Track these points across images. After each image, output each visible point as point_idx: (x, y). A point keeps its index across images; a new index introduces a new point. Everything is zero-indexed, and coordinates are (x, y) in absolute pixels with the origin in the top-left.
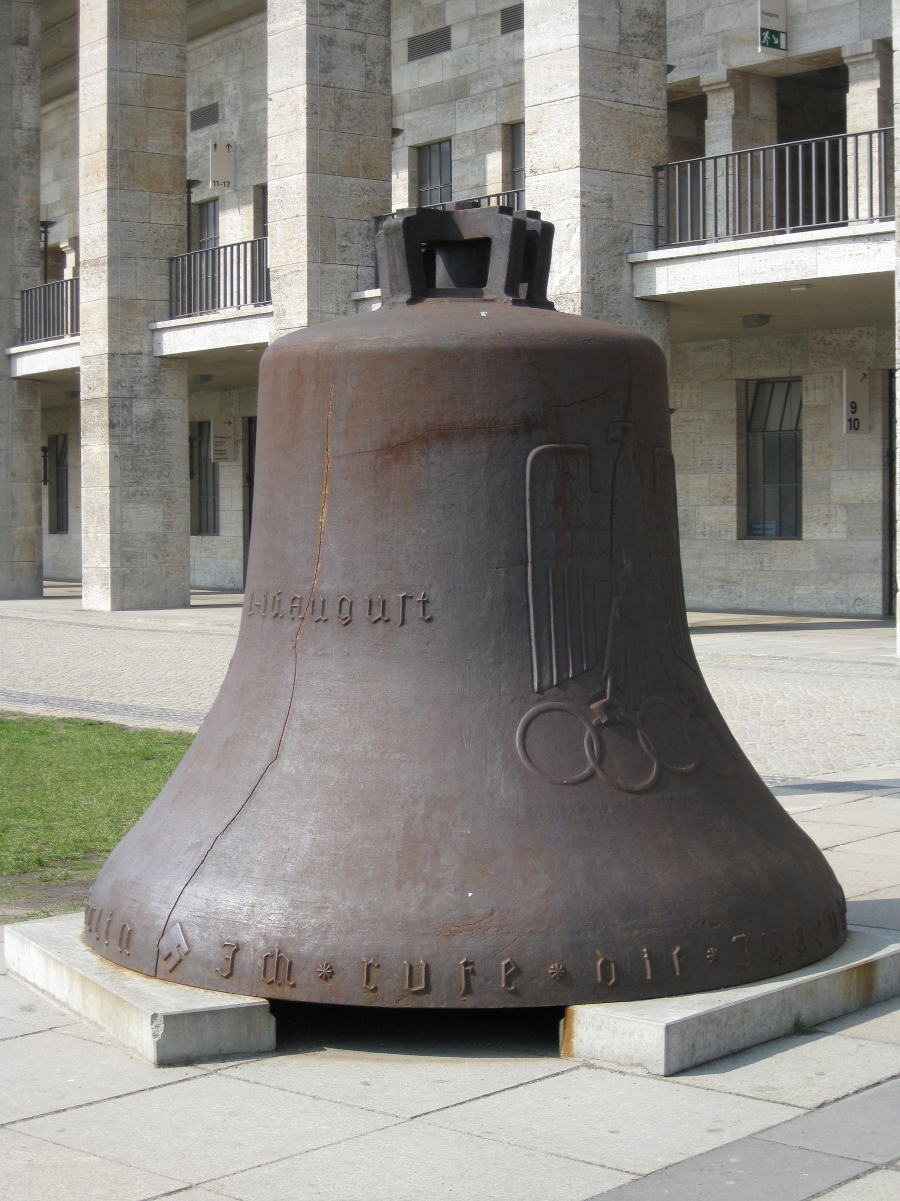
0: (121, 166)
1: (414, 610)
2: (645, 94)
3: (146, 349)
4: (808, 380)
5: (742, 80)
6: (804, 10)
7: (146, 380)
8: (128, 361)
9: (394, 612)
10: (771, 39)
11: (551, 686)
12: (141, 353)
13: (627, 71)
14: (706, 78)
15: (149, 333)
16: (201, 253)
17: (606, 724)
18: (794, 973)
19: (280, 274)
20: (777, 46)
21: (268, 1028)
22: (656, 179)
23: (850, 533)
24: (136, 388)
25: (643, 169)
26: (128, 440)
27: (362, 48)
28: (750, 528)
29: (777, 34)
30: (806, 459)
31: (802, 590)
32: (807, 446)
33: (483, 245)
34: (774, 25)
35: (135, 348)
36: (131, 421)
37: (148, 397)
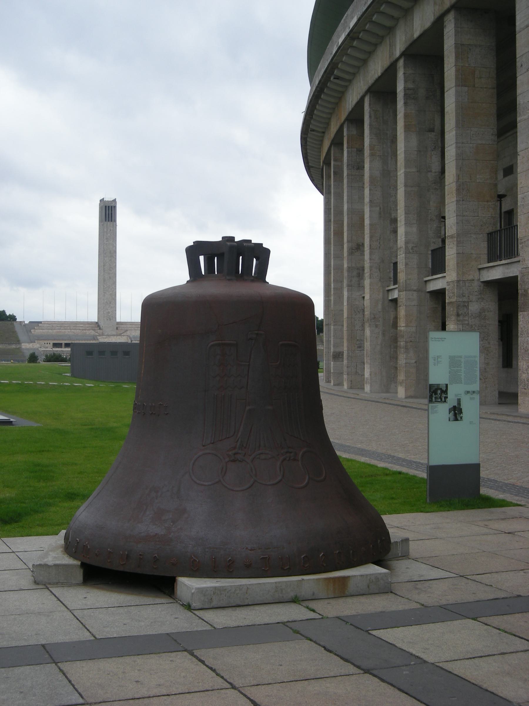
0: (463, 189)
3: (476, 278)
7: (476, 293)
8: (467, 284)
12: (473, 280)
15: (477, 271)
16: (509, 228)
19: (523, 241)
21: (79, 575)
24: (471, 297)
26: (466, 322)
35: (471, 277)
36: (468, 313)
37: (477, 301)
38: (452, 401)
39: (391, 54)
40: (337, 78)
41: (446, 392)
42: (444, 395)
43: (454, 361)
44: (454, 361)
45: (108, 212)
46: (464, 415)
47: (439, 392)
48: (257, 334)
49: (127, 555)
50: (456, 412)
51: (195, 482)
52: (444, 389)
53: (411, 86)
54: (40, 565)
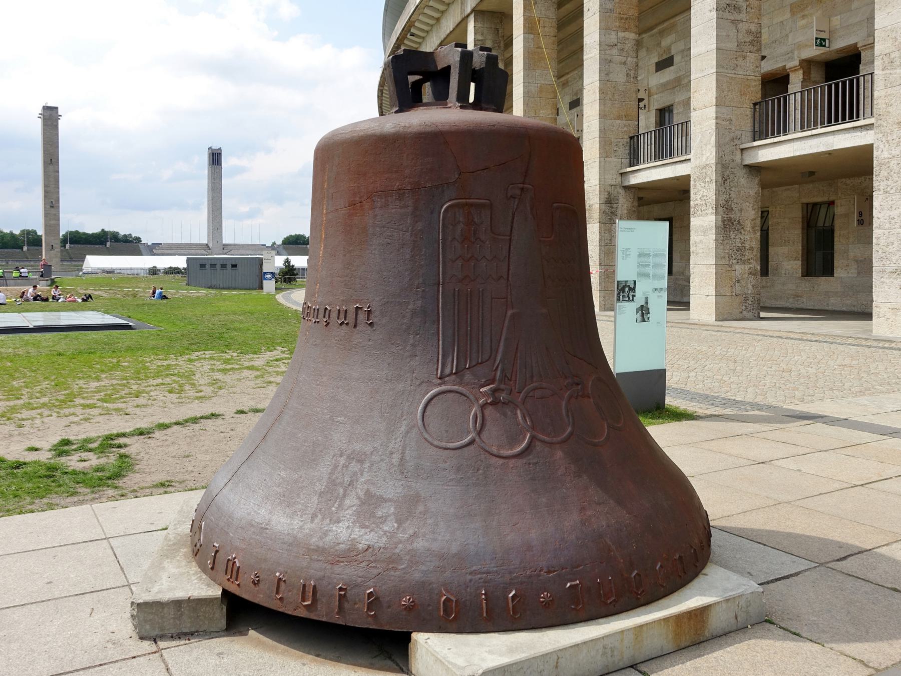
1: (362, 317)
2: (752, 70)
4: (838, 202)
5: (807, 65)
6: (838, 27)
9: (351, 318)
10: (821, 42)
11: (451, 374)
13: (740, 59)
14: (789, 65)
17: (491, 404)
18: (630, 612)
20: (825, 46)
21: (220, 616)
22: (755, 109)
23: (859, 273)
25: (748, 105)
27: (625, 63)
28: (808, 272)
29: (824, 40)
30: (836, 239)
31: (833, 301)
32: (836, 234)
33: (447, 69)
34: (822, 36)
38: (639, 300)
39: (463, 10)
40: (413, 35)
41: (633, 289)
42: (631, 294)
43: (643, 255)
44: (643, 255)
45: (215, 158)
46: (651, 315)
47: (627, 289)
48: (522, 189)
49: (314, 587)
50: (644, 312)
51: (432, 444)
52: (632, 286)
53: (480, 38)
54: (146, 604)
